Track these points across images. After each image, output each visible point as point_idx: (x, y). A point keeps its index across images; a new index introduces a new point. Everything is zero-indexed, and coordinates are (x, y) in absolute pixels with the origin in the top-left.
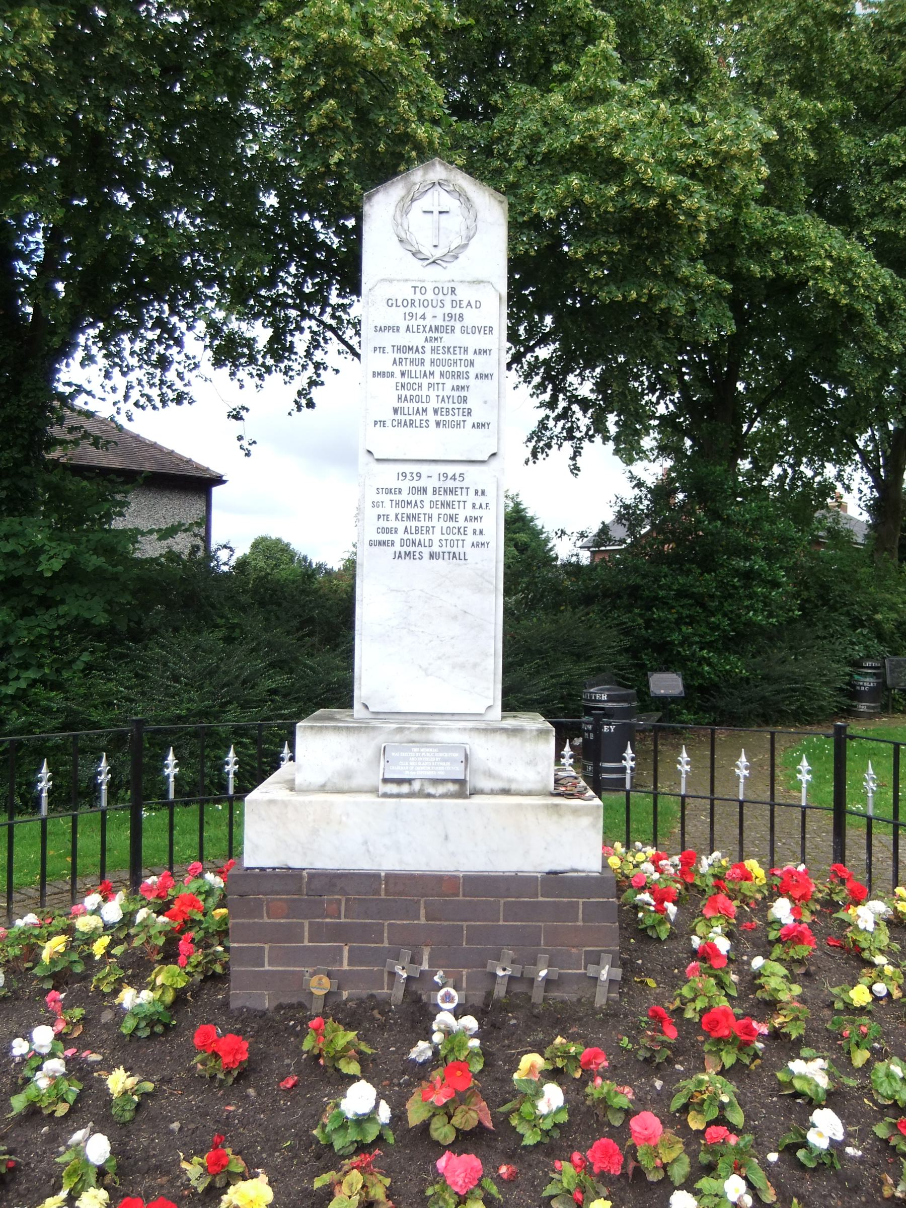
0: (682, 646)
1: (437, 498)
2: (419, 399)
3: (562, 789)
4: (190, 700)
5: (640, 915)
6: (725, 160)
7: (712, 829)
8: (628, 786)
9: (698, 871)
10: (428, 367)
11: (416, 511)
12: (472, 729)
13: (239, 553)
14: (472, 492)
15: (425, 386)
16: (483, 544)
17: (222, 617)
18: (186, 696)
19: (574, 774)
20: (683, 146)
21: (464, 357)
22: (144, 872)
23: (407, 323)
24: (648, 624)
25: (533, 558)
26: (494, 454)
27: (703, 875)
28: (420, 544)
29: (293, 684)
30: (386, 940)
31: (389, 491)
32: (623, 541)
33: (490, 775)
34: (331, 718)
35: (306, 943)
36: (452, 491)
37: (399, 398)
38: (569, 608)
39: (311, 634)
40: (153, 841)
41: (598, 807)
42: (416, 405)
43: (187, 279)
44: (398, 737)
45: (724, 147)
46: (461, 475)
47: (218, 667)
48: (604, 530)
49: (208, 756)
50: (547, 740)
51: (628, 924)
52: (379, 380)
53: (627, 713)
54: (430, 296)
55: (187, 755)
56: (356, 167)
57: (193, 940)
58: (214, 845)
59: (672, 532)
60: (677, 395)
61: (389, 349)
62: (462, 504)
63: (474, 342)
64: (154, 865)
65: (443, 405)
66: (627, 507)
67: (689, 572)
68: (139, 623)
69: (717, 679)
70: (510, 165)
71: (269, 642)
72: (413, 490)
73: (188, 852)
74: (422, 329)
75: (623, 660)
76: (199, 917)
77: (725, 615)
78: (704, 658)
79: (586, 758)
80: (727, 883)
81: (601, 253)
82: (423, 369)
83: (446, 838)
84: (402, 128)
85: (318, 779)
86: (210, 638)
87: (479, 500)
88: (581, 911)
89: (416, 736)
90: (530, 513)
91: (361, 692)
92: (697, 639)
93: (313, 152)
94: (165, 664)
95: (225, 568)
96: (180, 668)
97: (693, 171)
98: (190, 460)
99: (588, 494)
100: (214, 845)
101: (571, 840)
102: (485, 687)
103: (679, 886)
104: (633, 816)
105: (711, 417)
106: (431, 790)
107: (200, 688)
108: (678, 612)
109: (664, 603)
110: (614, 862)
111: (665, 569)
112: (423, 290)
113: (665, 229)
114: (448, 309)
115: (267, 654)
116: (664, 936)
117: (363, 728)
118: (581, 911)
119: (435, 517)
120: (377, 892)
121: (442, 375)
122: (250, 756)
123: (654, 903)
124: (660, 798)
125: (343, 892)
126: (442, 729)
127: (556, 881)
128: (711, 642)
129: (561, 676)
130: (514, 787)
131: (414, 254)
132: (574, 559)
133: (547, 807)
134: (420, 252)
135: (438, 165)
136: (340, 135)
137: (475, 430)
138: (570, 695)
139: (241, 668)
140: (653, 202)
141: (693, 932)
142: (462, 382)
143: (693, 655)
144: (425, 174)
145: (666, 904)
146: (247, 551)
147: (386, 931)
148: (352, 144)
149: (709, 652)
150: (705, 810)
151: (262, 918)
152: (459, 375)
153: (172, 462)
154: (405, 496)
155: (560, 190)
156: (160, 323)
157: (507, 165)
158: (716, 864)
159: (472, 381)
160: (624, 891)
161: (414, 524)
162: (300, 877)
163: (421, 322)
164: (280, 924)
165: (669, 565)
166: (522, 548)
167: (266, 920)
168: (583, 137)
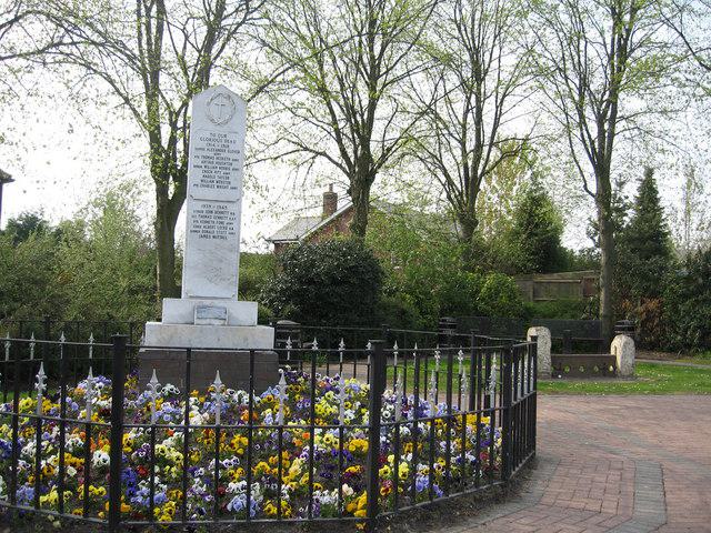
36: (222, 213)
154: (204, 214)
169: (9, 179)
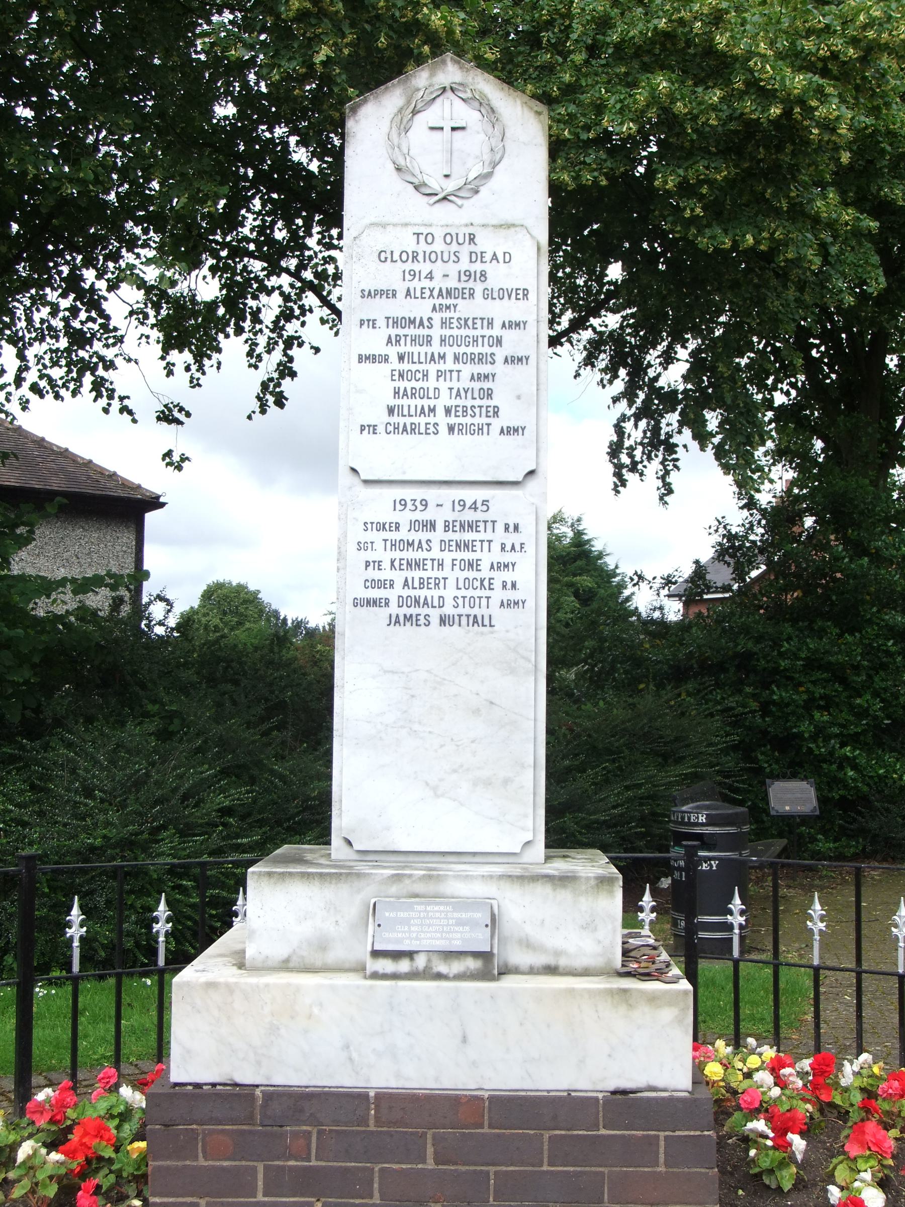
0: (815, 742)
1: (450, 535)
2: (424, 394)
3: (634, 965)
4: (107, 824)
5: (752, 1152)
6: (870, 51)
7: (859, 1017)
8: (736, 953)
9: (838, 1083)
10: (436, 348)
11: (420, 555)
12: (501, 877)
13: (181, 608)
14: (500, 527)
15: (432, 375)
16: (516, 603)
17: (154, 702)
18: (102, 817)
19: (651, 941)
20: (810, 32)
21: (487, 332)
22: (36, 1080)
23: (407, 284)
24: (765, 709)
25: (599, 612)
26: (531, 473)
27: (846, 1090)
28: (426, 603)
29: (255, 801)
30: (376, 1194)
31: (382, 527)
32: (726, 588)
33: (527, 944)
34: (299, 860)
35: (260, 1198)
36: (471, 526)
37: (396, 393)
38: (652, 687)
39: (280, 727)
40: (49, 1033)
41: (686, 992)
42: (419, 402)
43: (114, 222)
44: (394, 889)
45: (871, 34)
46: (485, 502)
47: (147, 775)
48: (700, 572)
49: (132, 906)
50: (611, 892)
51: (735, 1167)
52: (367, 366)
53: (732, 842)
54: (438, 246)
55: (102, 904)
56: (349, 65)
57: (98, 1187)
58: (138, 1039)
59: (798, 576)
60: (802, 378)
61: (381, 323)
62: (486, 545)
63: (502, 311)
64: (51, 1069)
65: (458, 402)
66: (731, 537)
67: (821, 633)
68: (38, 710)
69: (865, 789)
70: (565, 59)
71: (221, 738)
72: (415, 525)
73: (101, 1050)
74: (428, 293)
75: (730, 762)
76: (108, 1153)
77: (876, 694)
78: (847, 758)
79: (677, 908)
80: (880, 1102)
81: (700, 183)
82: (429, 350)
83: (464, 1040)
84: (410, 14)
85: (279, 952)
86: (133, 732)
87: (511, 539)
88: (662, 1150)
89: (419, 888)
90: (597, 546)
91: (343, 819)
92: (836, 730)
93: (288, 47)
94: (73, 771)
95: (160, 630)
96: (94, 776)
97: (826, 67)
98: (115, 474)
99: (675, 527)
100: (138, 1039)
101: (644, 1043)
102: (520, 818)
103: (809, 1107)
104: (744, 996)
105: (851, 408)
106: (442, 968)
107: (123, 805)
108: (807, 691)
109: (788, 679)
110: (714, 1070)
111: (788, 629)
112: (430, 238)
113: (789, 148)
114: (464, 264)
115: (218, 756)
116: (787, 1186)
117: (343, 875)
118: (662, 1150)
119: (448, 563)
120: (364, 1121)
121: (456, 358)
122: (192, 906)
123: (772, 1135)
124: (783, 970)
125: (314, 1121)
126: (458, 877)
127: (624, 1103)
128: (856, 734)
129: (639, 786)
130: (563, 962)
131: (416, 188)
132: (657, 615)
133: (611, 992)
134: (425, 185)
135: (449, 63)
136: (327, 24)
137: (505, 439)
138: (653, 814)
139: (181, 777)
140: (775, 111)
141: (830, 1179)
142: (485, 369)
143: (831, 753)
144: (432, 75)
145: (790, 1136)
146: (196, 604)
147: (376, 1179)
148: (343, 36)
149: (854, 749)
150: (850, 986)
151: (196, 1158)
152: (480, 359)
153: (89, 477)
154: (404, 534)
155: (641, 96)
156: (73, 284)
157: (560, 60)
158: (864, 1072)
159: (499, 368)
160: (730, 1115)
161: (417, 574)
162: (252, 1096)
163: (426, 283)
164: (223, 1169)
165: (794, 621)
166: (585, 597)
167: (202, 1162)
168: (670, 21)
169: (155, 503)
